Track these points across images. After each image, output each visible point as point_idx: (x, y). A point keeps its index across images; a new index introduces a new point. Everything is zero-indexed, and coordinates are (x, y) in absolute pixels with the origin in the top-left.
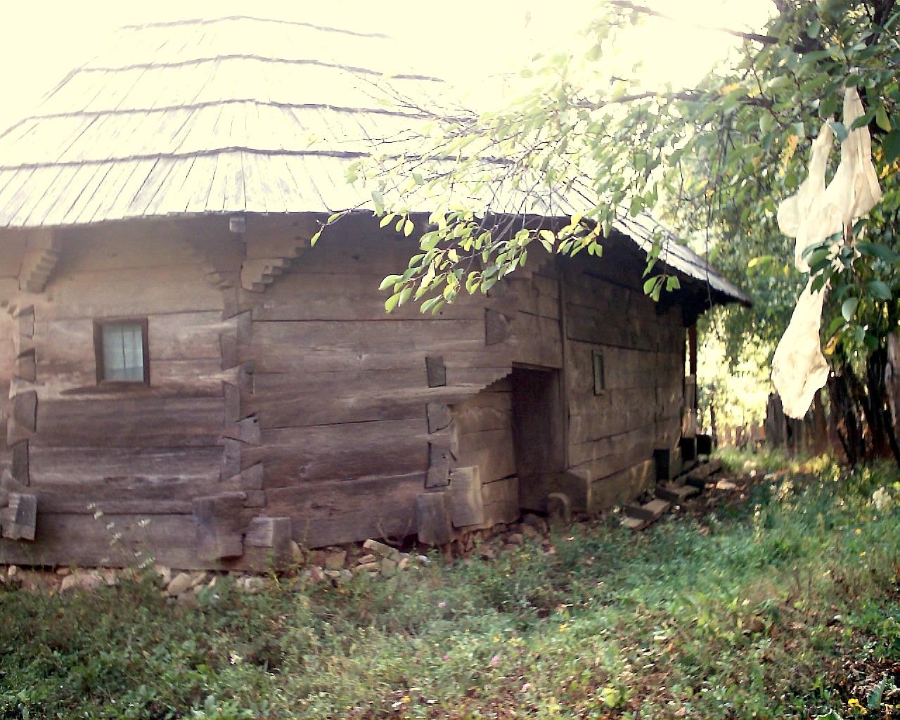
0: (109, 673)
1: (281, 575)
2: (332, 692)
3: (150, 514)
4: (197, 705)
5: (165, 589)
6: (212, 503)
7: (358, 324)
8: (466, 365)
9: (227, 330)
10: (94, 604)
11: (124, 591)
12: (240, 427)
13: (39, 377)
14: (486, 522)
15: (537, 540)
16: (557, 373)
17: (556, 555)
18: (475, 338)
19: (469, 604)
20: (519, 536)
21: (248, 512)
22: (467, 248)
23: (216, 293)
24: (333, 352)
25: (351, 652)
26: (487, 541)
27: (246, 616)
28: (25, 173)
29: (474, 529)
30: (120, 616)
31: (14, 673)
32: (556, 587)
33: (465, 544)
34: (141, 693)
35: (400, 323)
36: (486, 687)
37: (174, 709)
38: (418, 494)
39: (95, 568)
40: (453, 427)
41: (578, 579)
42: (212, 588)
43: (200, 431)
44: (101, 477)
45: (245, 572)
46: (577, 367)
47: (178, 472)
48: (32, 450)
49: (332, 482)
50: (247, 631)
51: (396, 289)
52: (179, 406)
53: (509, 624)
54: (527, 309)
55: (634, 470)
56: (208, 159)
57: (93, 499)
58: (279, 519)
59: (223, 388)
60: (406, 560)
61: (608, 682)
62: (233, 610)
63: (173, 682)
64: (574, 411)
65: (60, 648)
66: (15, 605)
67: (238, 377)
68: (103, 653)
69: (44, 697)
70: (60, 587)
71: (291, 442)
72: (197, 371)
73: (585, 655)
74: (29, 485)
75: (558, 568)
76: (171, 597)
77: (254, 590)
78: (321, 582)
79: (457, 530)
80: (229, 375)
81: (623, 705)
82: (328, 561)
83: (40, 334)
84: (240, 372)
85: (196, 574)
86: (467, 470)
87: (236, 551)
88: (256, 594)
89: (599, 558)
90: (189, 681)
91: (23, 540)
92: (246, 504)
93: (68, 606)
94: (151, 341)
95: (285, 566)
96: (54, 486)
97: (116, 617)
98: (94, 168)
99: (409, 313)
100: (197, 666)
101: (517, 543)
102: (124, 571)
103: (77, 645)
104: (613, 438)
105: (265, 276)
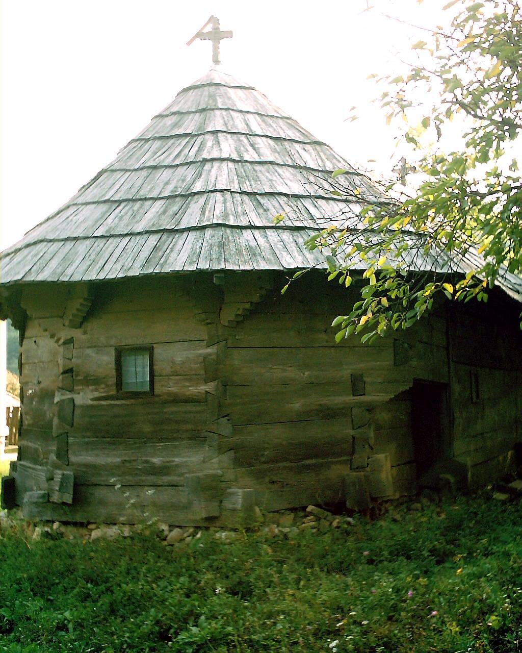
0: (129, 599)
1: (248, 530)
2: (289, 616)
3: (155, 486)
4: (191, 623)
5: (165, 539)
6: (198, 478)
7: (303, 350)
8: (380, 380)
9: (210, 355)
10: (116, 549)
11: (136, 541)
12: (218, 423)
13: (76, 388)
14: (394, 495)
15: (432, 508)
16: (446, 387)
17: (446, 519)
18: (386, 360)
19: (386, 553)
20: (419, 505)
21: (223, 485)
22: (393, 297)
23: (203, 328)
24: (284, 371)
25: (300, 587)
26: (396, 507)
27: (224, 560)
28: (69, 245)
29: (385, 499)
30: (134, 558)
31: (61, 597)
32: (448, 543)
33: (380, 510)
34: (151, 614)
35: (333, 350)
36: (403, 614)
37: (176, 626)
38: (345, 473)
39: (115, 524)
40: (370, 425)
41: (464, 537)
42: (199, 539)
43: (189, 427)
44: (119, 460)
45: (222, 528)
46: (459, 382)
47: (175, 456)
48: (71, 440)
49: (285, 464)
50: (224, 570)
51: (343, 325)
52: (173, 409)
53: (415, 569)
54: (425, 340)
55: (501, 458)
56: (198, 232)
57: (113, 475)
58: (246, 490)
59: (206, 396)
60: (337, 520)
61: (493, 611)
62: (213, 555)
63: (174, 606)
64: (457, 415)
65: (92, 582)
66: (59, 550)
67: (217, 388)
68: (124, 585)
69: (83, 616)
70: (89, 538)
71: (254, 436)
72: (187, 384)
73: (475, 592)
74: (68, 465)
75: (448, 529)
76: (170, 545)
77: (228, 541)
78: (275, 536)
79: (374, 500)
80: (210, 387)
81: (505, 628)
82: (282, 521)
83: (77, 357)
84: (218, 384)
85: (187, 529)
86: (381, 456)
87: (216, 514)
88: (230, 544)
89: (478, 522)
90: (185, 606)
91: (64, 504)
92: (222, 479)
93: (96, 551)
94: (155, 363)
95: (250, 524)
96: (87, 466)
97: (131, 559)
98: (118, 240)
99: (350, 344)
100: (191, 595)
101: (417, 510)
102: (136, 526)
103: (104, 579)
104: (486, 435)
105: (237, 315)
